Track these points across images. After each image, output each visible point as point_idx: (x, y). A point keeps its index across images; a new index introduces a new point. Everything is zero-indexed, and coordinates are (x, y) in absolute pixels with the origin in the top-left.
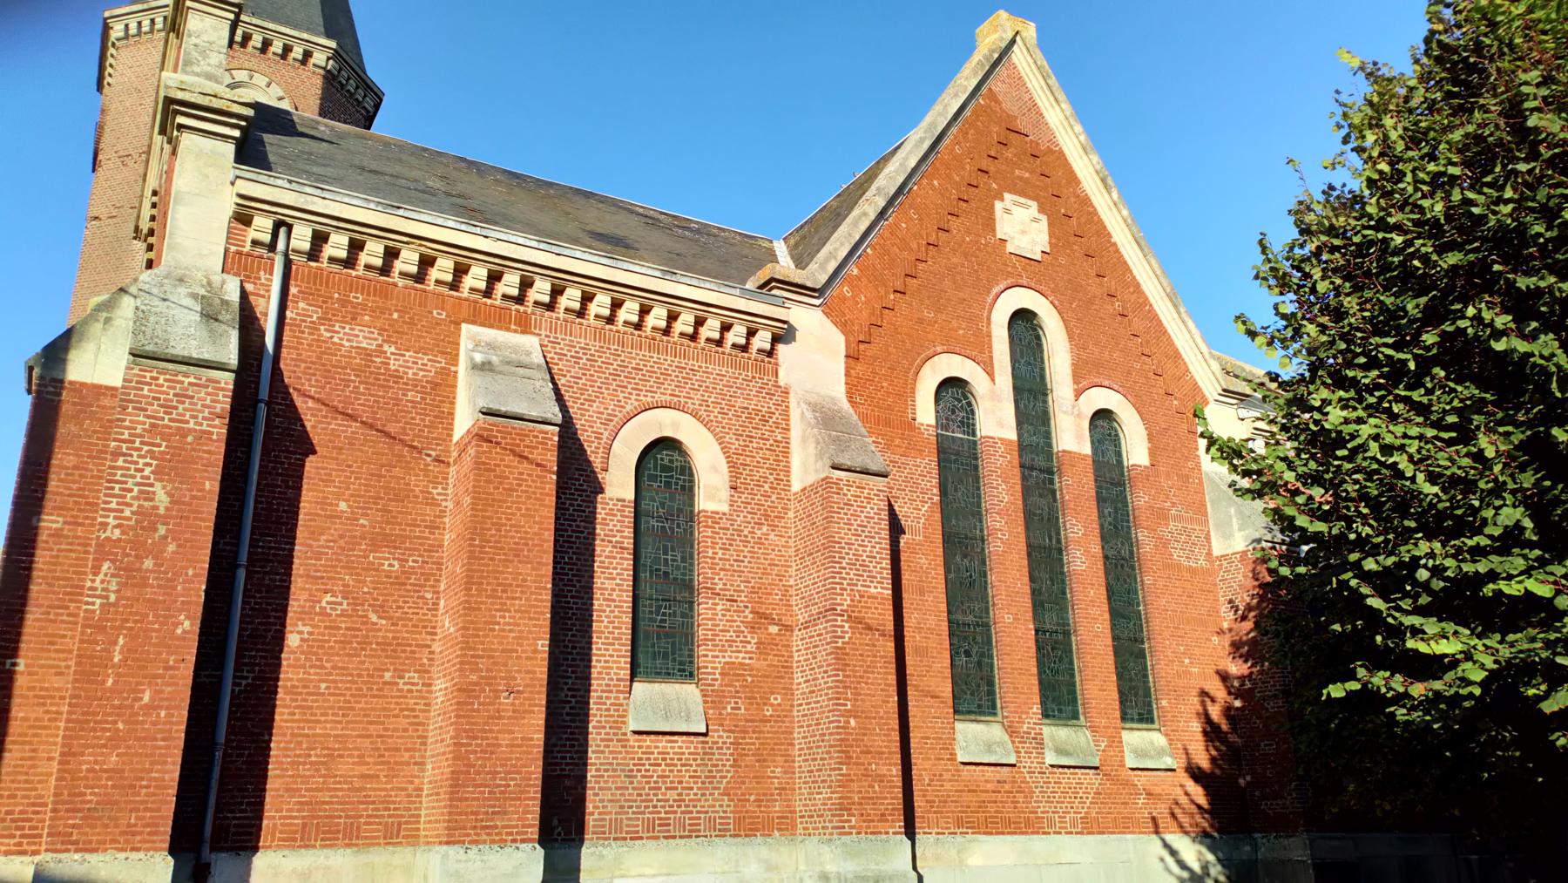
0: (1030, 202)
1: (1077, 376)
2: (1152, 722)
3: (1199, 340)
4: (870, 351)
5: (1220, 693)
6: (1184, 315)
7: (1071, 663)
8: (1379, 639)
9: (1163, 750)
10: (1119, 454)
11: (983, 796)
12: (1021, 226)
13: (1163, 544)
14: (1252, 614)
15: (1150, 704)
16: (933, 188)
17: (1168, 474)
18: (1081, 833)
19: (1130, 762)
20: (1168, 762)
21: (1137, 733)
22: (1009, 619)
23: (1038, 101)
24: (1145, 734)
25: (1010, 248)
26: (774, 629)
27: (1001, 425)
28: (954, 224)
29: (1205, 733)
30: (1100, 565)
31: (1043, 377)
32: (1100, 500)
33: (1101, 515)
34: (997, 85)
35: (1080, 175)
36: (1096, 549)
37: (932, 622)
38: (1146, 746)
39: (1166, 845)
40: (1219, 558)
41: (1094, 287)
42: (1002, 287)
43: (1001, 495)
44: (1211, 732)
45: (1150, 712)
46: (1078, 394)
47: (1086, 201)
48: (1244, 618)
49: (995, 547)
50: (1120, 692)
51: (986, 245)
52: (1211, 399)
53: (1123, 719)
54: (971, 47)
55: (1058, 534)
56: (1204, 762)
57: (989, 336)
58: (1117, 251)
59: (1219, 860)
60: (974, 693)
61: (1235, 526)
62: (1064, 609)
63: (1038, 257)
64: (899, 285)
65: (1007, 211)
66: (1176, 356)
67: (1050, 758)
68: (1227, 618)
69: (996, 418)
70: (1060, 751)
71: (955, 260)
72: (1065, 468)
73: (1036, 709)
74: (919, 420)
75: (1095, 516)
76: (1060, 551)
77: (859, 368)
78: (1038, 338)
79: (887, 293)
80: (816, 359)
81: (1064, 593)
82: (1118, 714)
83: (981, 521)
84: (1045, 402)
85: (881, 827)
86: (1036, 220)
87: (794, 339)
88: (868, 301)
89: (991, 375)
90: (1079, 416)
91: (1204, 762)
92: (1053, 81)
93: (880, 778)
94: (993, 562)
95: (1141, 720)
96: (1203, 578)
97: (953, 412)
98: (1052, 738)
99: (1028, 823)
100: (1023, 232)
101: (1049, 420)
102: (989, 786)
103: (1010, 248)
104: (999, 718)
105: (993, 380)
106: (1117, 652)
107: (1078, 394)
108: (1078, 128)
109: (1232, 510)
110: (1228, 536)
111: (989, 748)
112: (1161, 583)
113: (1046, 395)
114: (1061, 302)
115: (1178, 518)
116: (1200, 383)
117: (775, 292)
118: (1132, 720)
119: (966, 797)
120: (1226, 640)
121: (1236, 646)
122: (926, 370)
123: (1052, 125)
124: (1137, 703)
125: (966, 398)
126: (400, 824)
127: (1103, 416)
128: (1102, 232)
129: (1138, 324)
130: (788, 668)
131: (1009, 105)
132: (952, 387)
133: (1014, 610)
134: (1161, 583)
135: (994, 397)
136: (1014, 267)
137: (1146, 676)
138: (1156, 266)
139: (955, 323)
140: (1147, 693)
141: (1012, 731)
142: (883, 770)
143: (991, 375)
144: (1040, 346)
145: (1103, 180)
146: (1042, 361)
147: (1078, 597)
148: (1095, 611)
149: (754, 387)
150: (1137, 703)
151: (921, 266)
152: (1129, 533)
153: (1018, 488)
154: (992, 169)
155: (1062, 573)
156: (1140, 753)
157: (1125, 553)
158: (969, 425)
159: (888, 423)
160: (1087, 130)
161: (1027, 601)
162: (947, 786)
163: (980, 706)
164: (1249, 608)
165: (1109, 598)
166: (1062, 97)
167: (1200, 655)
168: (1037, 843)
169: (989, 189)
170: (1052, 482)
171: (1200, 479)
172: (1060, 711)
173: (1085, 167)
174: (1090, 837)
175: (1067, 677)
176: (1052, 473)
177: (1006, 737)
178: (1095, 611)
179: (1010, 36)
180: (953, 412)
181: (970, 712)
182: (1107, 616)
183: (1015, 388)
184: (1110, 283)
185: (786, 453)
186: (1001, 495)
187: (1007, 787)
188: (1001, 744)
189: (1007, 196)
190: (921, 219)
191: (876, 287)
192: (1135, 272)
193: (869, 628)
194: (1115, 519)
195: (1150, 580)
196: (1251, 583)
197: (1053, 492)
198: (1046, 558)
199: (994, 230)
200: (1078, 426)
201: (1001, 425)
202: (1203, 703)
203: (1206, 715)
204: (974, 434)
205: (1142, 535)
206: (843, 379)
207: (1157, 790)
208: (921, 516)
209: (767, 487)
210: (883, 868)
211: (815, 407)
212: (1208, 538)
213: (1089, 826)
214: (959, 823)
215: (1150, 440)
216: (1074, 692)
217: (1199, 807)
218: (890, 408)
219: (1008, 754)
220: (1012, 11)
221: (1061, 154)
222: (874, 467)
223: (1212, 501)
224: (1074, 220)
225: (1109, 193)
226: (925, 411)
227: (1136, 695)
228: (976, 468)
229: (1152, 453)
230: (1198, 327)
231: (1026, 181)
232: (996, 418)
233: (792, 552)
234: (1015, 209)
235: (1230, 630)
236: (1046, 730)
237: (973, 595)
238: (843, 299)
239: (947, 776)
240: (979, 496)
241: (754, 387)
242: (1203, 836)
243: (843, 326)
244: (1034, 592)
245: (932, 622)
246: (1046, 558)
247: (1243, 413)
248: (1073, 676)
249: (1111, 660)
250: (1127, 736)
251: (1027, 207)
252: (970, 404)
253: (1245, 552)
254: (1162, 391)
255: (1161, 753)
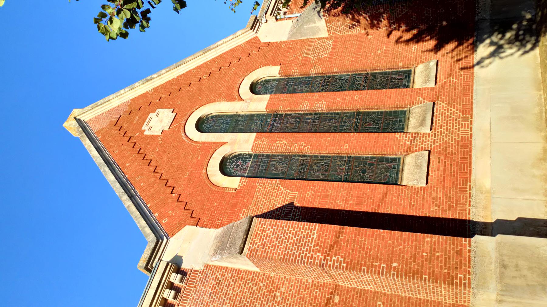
0: (149, 117)
1: (232, 99)
2: (410, 71)
3: (225, 40)
4: (197, 211)
5: (396, 34)
6: (214, 46)
7: (374, 113)
8: (444, 23)
9: (427, 66)
10: (274, 80)
11: (447, 173)
12: (159, 122)
13: (319, 61)
14: (356, 18)
15: (400, 72)
16: (130, 166)
17: (286, 57)
18: (472, 115)
19: (432, 85)
20: (433, 64)
21: (416, 80)
22: (346, 146)
23: (107, 110)
24: (416, 75)
25: (166, 129)
26: (337, 299)
27: (247, 141)
28: (149, 157)
29: (417, 42)
30: (325, 94)
31: (231, 116)
32: (294, 92)
33: (301, 92)
34: (94, 129)
35: (144, 92)
36: (317, 95)
37: (343, 192)
38: (423, 77)
39: (478, 63)
40: (329, 34)
41: (194, 88)
42: (183, 134)
43: (283, 144)
44: (417, 39)
45: (405, 72)
46: (241, 99)
47: (156, 89)
48: (358, 21)
49: (308, 150)
50: (392, 88)
51: (162, 140)
52: (255, 35)
53: (407, 87)
54: (77, 139)
55: (307, 114)
56: (432, 43)
57: (203, 143)
58: (181, 76)
59: (489, 37)
60: (386, 172)
61: (313, 25)
62: (346, 114)
63: (174, 114)
64: (169, 190)
65: (150, 129)
66: (233, 51)
67: (426, 130)
68: (358, 31)
69: (243, 143)
70: (422, 123)
71: (165, 158)
72: (274, 109)
73: (398, 135)
74: (236, 187)
75: (300, 95)
76: (316, 114)
77: (204, 219)
78: (212, 117)
79: (172, 197)
80: (193, 245)
81: (338, 114)
82: (404, 90)
83: (295, 156)
84: (243, 116)
85: (465, 254)
86: (158, 115)
87: (181, 257)
88: (173, 210)
89: (223, 144)
90: (251, 99)
91: (432, 43)
92: (99, 102)
93: (433, 250)
94: (316, 151)
95: (409, 77)
96: (338, 42)
97: (238, 166)
98: (414, 127)
99: (465, 147)
100: (161, 121)
101: (251, 115)
102: (441, 168)
103: (166, 129)
104: (402, 157)
105: (225, 143)
106: (371, 88)
107: (241, 99)
108: (122, 91)
109: (305, 26)
110: (318, 29)
111: (418, 166)
112: (338, 63)
113: (239, 115)
114: (197, 104)
115: (308, 52)
116: (247, 40)
117: (154, 266)
118: (409, 82)
119: (447, 184)
120: (371, 31)
121: (372, 26)
122: (213, 179)
123: (119, 104)
124: (400, 79)
125: (233, 158)
126: (462, 173)
127: (254, 89)
128: (170, 83)
129: (215, 68)
130: (362, 293)
131: (104, 124)
132: (224, 168)
133: (342, 143)
134: (338, 63)
135: (233, 143)
136: (176, 127)
137: (386, 73)
138: (190, 58)
139: (194, 161)
140: (396, 73)
141: (408, 151)
142: (427, 247)
143: (223, 144)
144: (216, 116)
145: (147, 81)
146: (224, 116)
147: (339, 107)
148: (348, 99)
149: (200, 287)
150: (400, 79)
151: (163, 177)
152: (312, 78)
153: (280, 134)
154: (130, 135)
155: (327, 114)
156: (427, 80)
157: (320, 80)
158: (245, 158)
159: (235, 205)
160: (123, 87)
161: (338, 135)
162: (440, 195)
163: (394, 168)
164: (353, 19)
165: (342, 90)
166: (107, 98)
167: (377, 45)
168: (477, 143)
169: (138, 137)
170: (281, 115)
171: (291, 41)
172: (400, 121)
173: (141, 88)
174: (474, 110)
175: (382, 116)
176: (277, 115)
177: (413, 155)
178: (348, 99)
179: (75, 121)
180: (238, 166)
181: (397, 174)
182: (351, 92)
183: (233, 132)
184: (194, 80)
185: (239, 271)
186: (283, 144)
187: (442, 157)
188: (416, 158)
189: (143, 128)
190: (142, 175)
191: (167, 204)
192: (192, 68)
193: (336, 242)
194: (304, 84)
195: (336, 69)
196: (341, 19)
197: (286, 115)
198: (318, 123)
199: (157, 136)
200: (256, 100)
201: (247, 141)
202: (401, 42)
203: (408, 41)
204: (251, 155)
205: (313, 72)
206: (208, 229)
207: (448, 70)
208: (282, 193)
209: (255, 288)
210: (494, 259)
211: (215, 253)
212: (319, 39)
213: (468, 110)
214: (464, 190)
215: (268, 65)
216: (391, 112)
217: (457, 47)
218: (228, 203)
219: (423, 155)
220: (65, 119)
221: (133, 100)
222: (245, 227)
223: (302, 36)
224: (163, 96)
225: (154, 78)
226: (233, 183)
227: (395, 79)
228: (268, 156)
229: (274, 64)
230: (220, 40)
231: (140, 118)
232: (243, 143)
233: (293, 278)
234: (150, 125)
235: (365, 29)
236: (411, 130)
237: (332, 164)
238: (168, 223)
239: (434, 194)
240: (282, 156)
241: (200, 287)
242: (474, 47)
243: (181, 226)
244: (335, 131)
245: (343, 192)
246: (318, 123)
247: (264, 20)
248: (382, 113)
249: (375, 92)
250: (417, 85)
251: (151, 118)
252: (236, 156)
253: (326, 21)
254: (248, 58)
255: (427, 68)
